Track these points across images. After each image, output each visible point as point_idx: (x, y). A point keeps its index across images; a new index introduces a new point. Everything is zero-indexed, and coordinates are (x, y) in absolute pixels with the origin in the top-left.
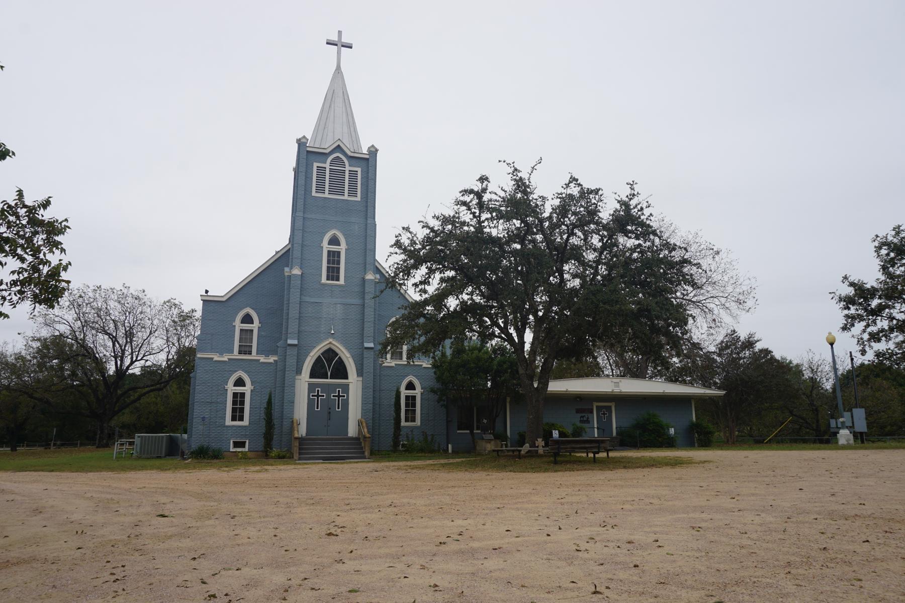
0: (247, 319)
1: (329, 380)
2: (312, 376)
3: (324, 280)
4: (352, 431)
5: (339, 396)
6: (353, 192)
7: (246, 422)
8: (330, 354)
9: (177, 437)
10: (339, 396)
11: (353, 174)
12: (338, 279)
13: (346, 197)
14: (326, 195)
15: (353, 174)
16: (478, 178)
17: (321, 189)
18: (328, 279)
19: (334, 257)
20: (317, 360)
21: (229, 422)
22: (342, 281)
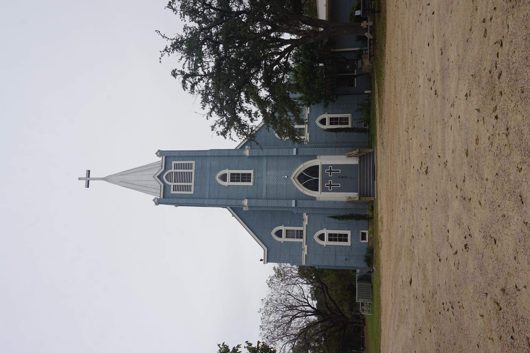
1: (320, 178)
2: (316, 189)
3: (251, 184)
4: (354, 161)
5: (331, 171)
6: (189, 166)
8: (301, 178)
10: (331, 171)
11: (177, 167)
12: (250, 174)
13: (193, 171)
14: (192, 184)
15: (177, 167)
17: (188, 188)
18: (250, 181)
22: (251, 172)
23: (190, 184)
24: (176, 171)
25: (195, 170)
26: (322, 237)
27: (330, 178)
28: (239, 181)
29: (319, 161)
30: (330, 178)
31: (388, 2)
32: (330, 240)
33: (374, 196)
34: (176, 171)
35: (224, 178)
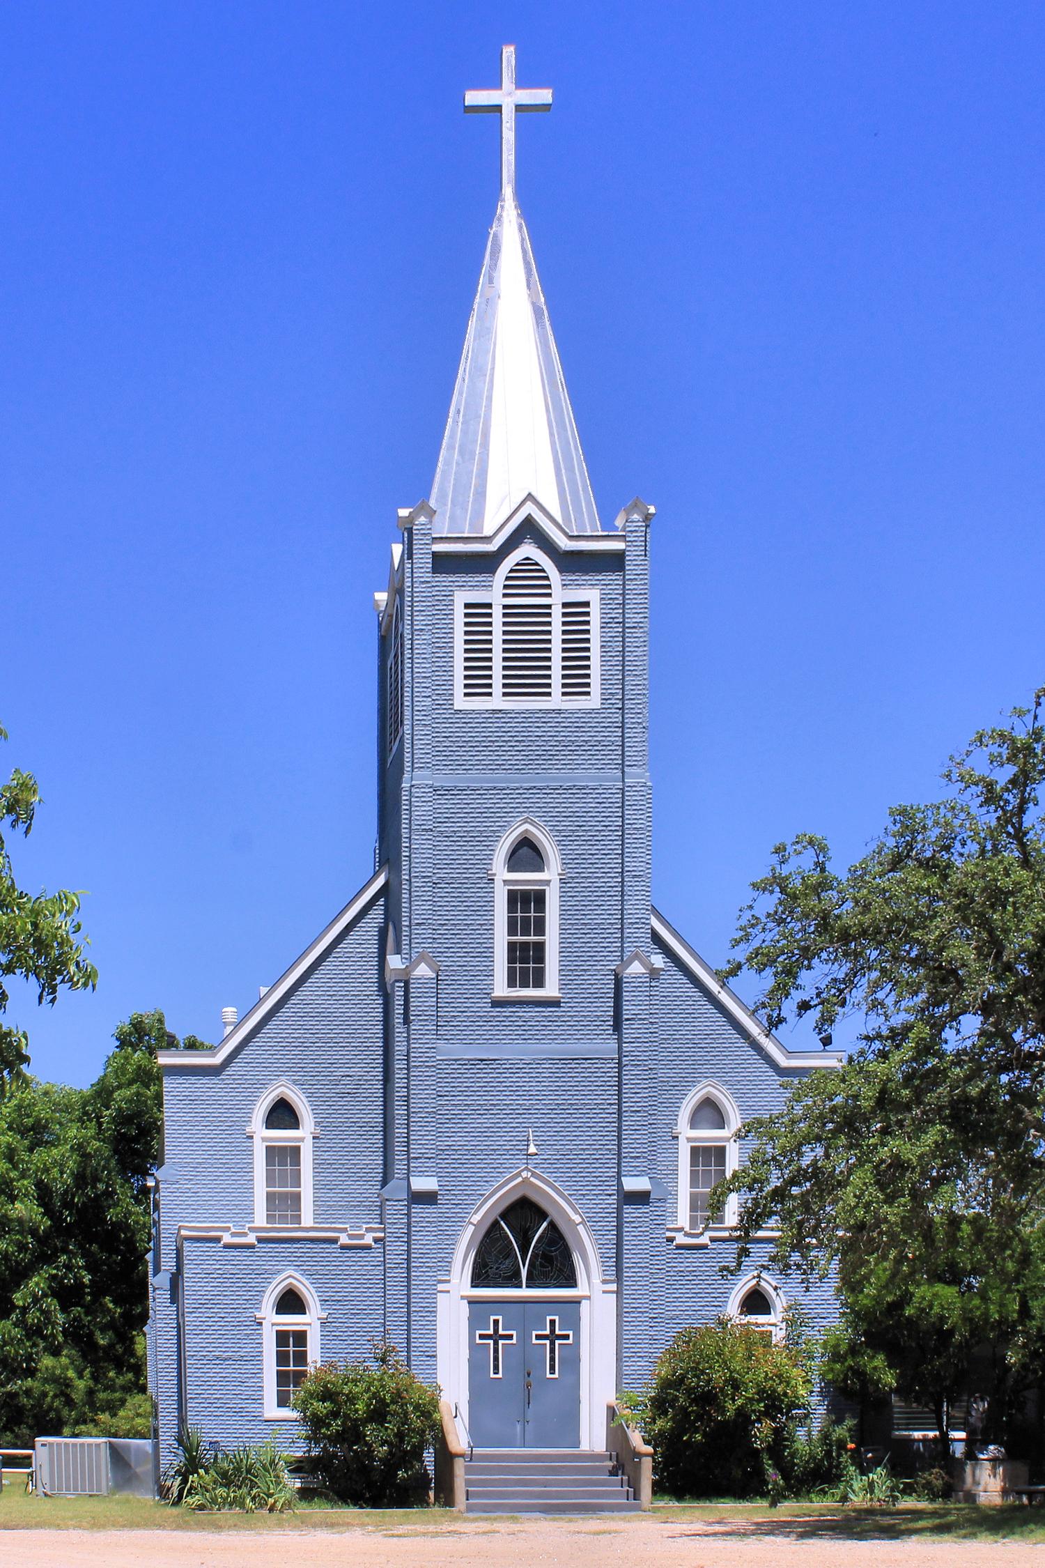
0: (282, 1114)
1: (525, 1292)
2: (480, 1277)
3: (501, 989)
4: (593, 1437)
5: (553, 1337)
6: (576, 683)
7: (514, 1333)
8: (524, 1212)
9: (128, 1447)
10: (553, 1337)
11: (575, 610)
12: (539, 982)
13: (556, 700)
14: (498, 701)
15: (575, 610)
16: (895, 806)
17: (478, 684)
18: (511, 983)
19: (527, 905)
20: (488, 1233)
21: (557, 1318)
22: (551, 989)
23: (497, 689)
24: (557, 611)
25: (559, 712)
26: (291, 1302)
27: (524, 1337)
28: (512, 930)
29: (592, 1286)
30: (524, 1337)
31: (1041, 1533)
32: (282, 1337)
33: (470, 1509)
34: (557, 611)
35: (526, 853)
